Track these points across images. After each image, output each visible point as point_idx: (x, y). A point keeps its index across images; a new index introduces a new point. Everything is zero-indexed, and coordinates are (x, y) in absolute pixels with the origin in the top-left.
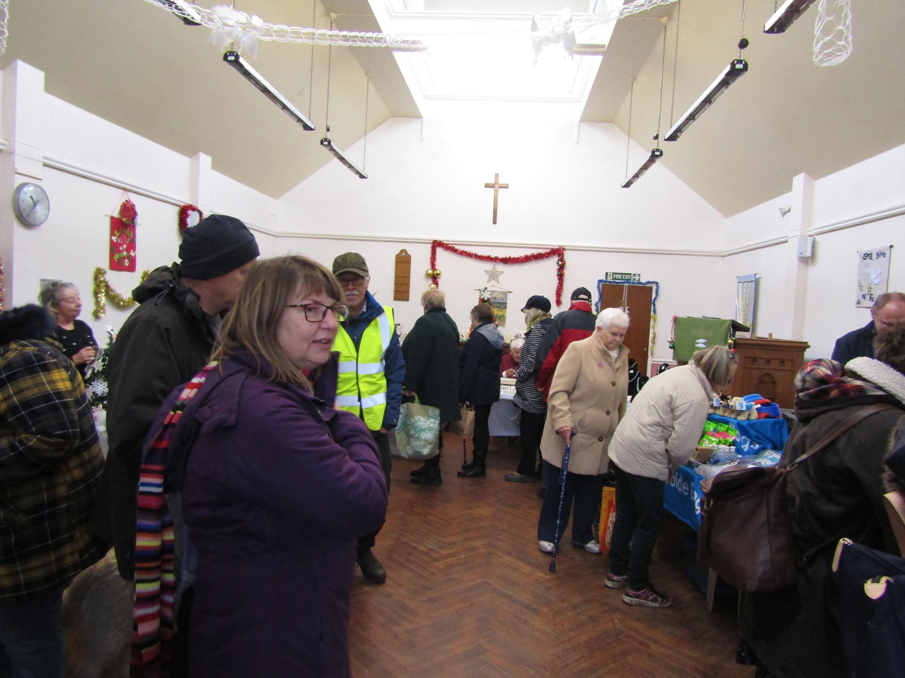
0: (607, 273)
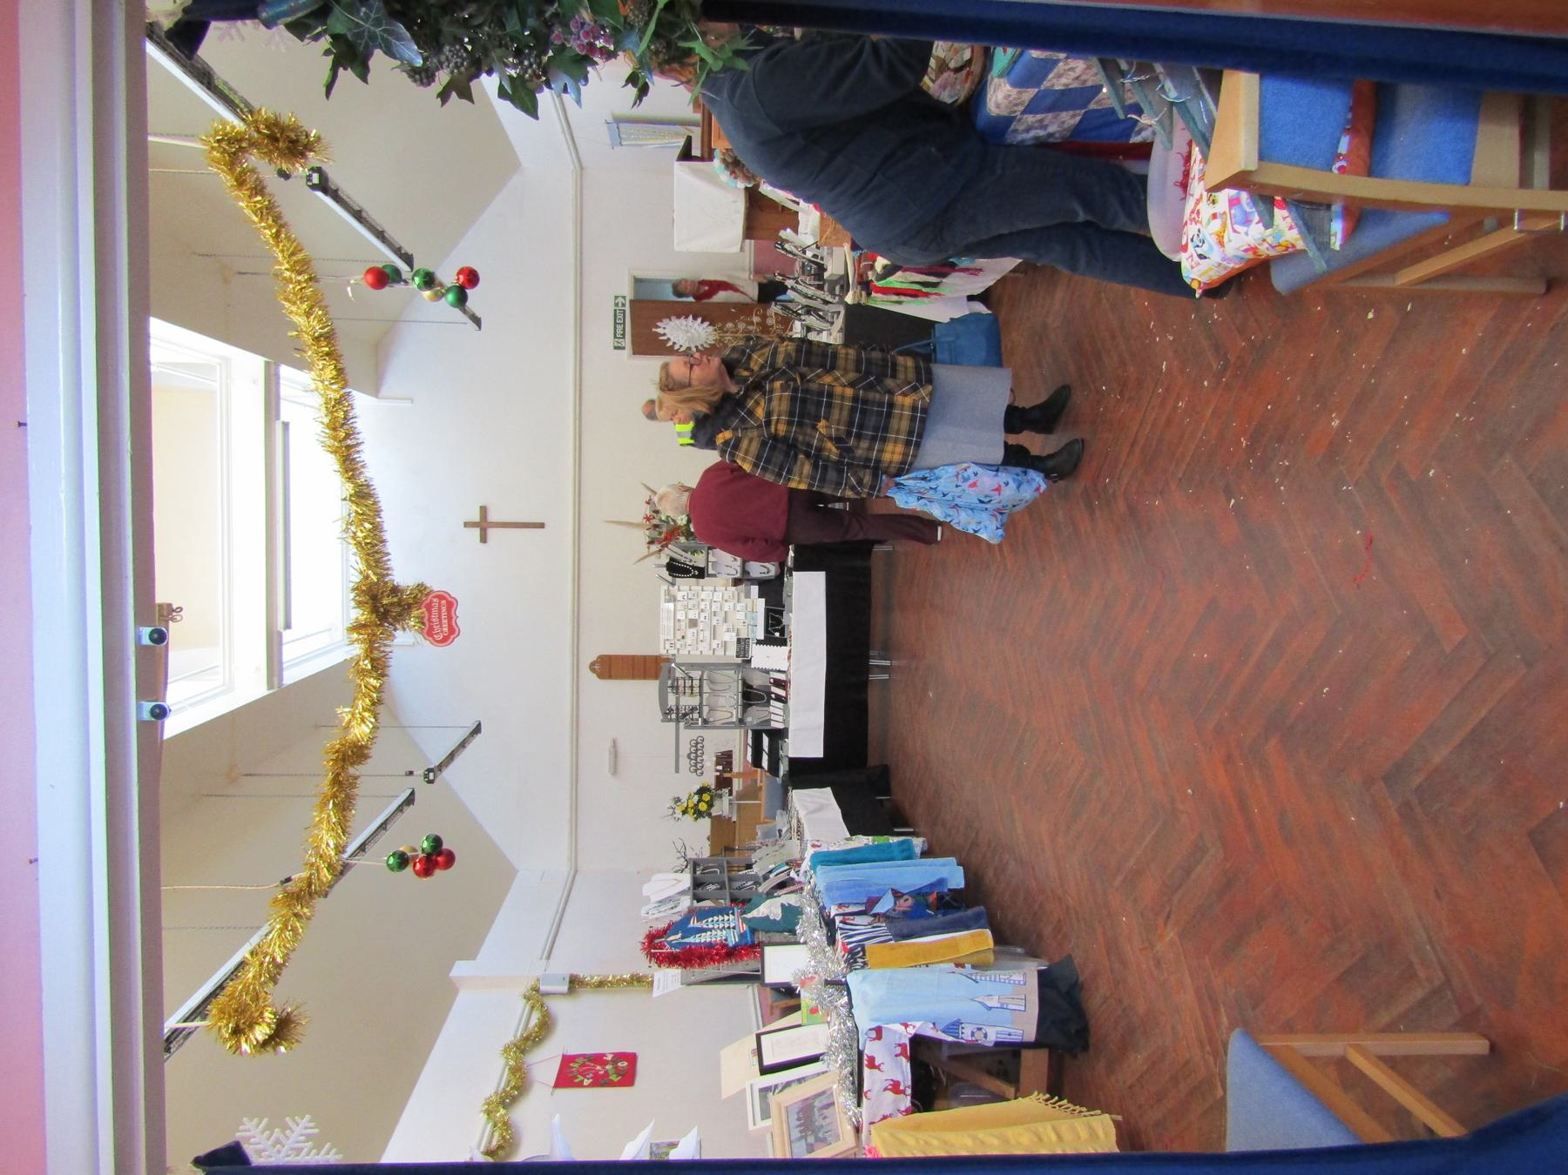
0: (616, 348)
